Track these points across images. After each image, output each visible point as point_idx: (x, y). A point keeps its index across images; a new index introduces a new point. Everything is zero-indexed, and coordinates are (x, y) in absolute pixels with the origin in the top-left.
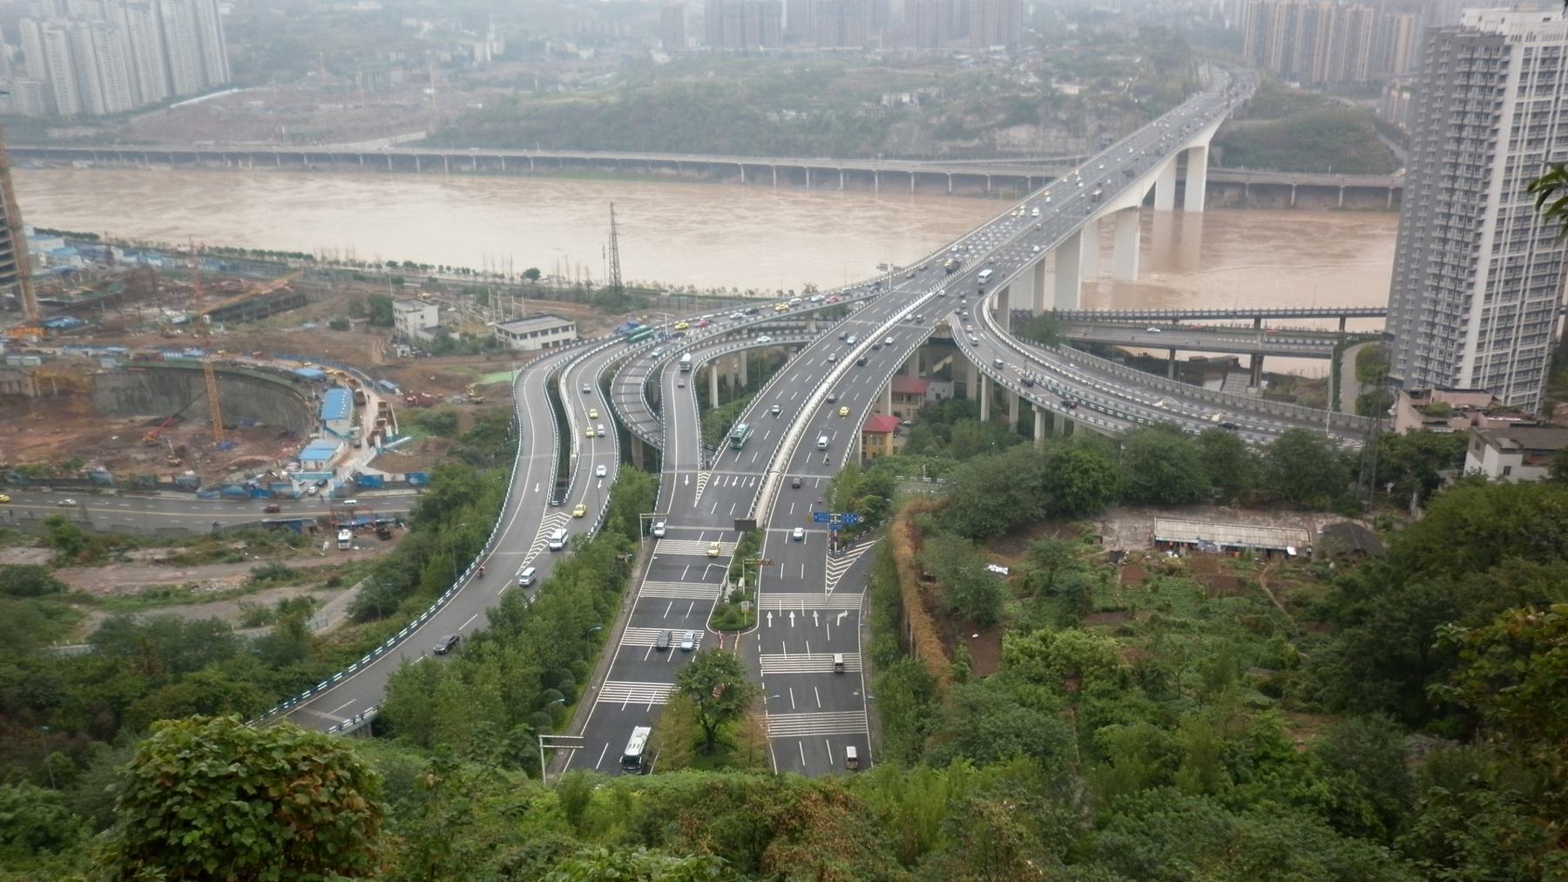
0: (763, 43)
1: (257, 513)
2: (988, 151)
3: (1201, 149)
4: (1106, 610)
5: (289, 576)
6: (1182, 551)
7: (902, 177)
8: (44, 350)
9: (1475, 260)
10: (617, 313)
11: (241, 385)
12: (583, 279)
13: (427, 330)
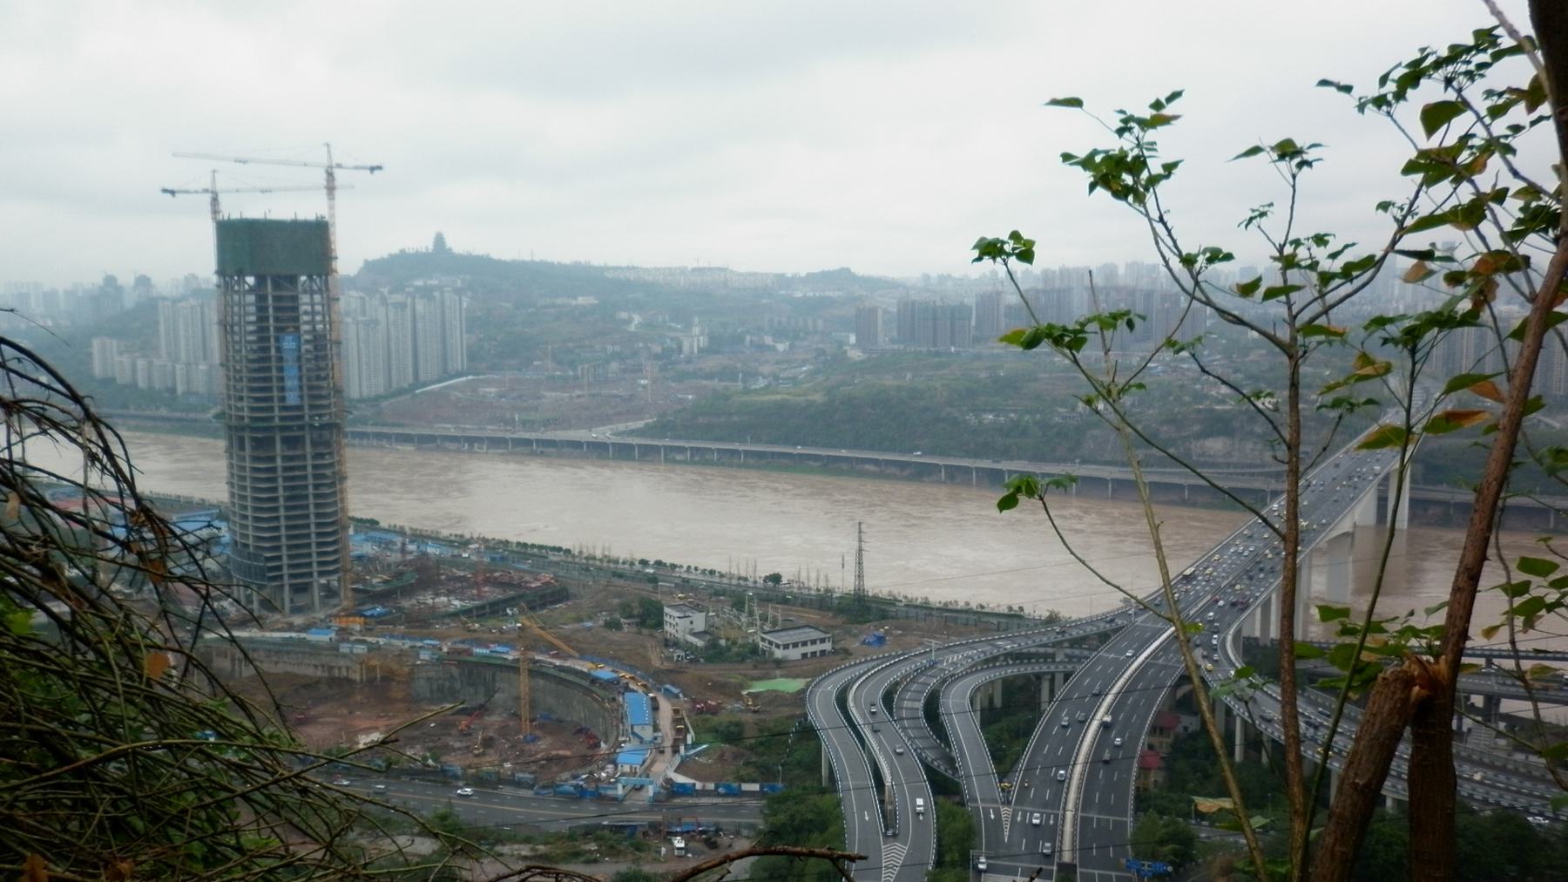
0: (953, 343)
1: (586, 813)
11: (541, 682)
12: (822, 585)
13: (695, 635)
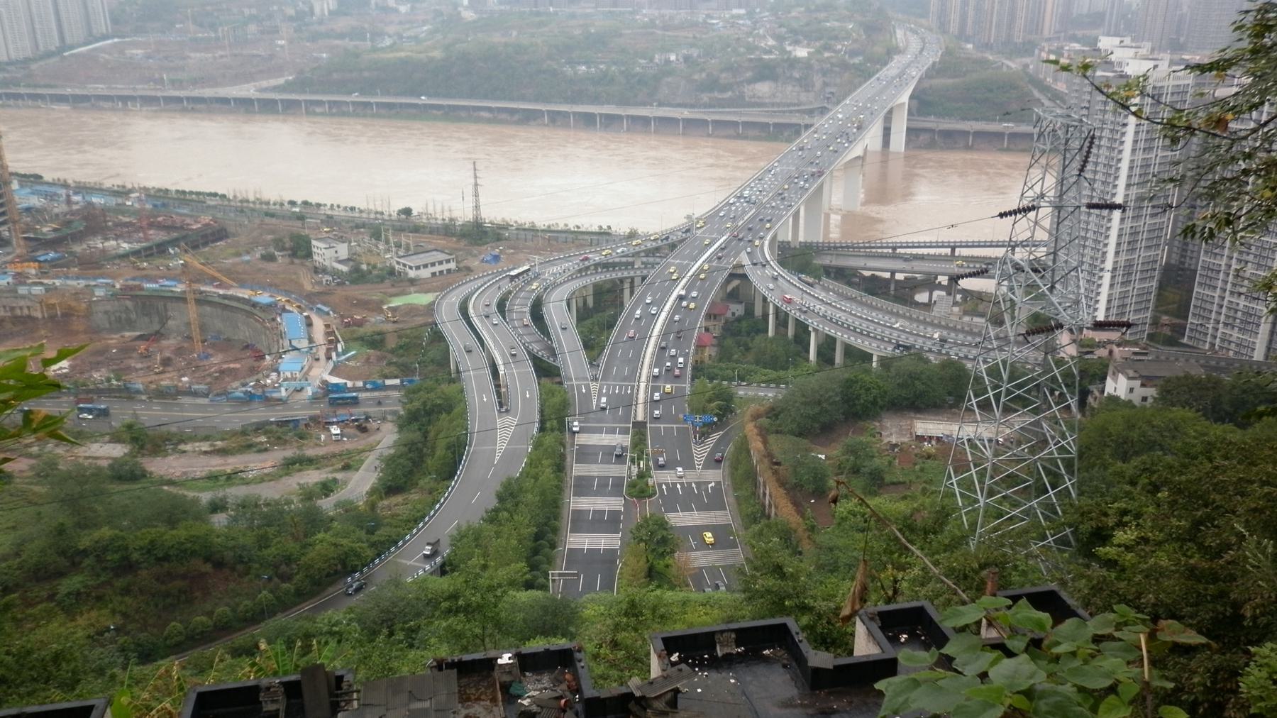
2: (740, 102)
4: (893, 484)
5: (310, 462)
6: (934, 442)
8: (46, 281)
9: (1108, 228)
10: (480, 245)
11: (208, 309)
12: (447, 215)
13: (340, 262)
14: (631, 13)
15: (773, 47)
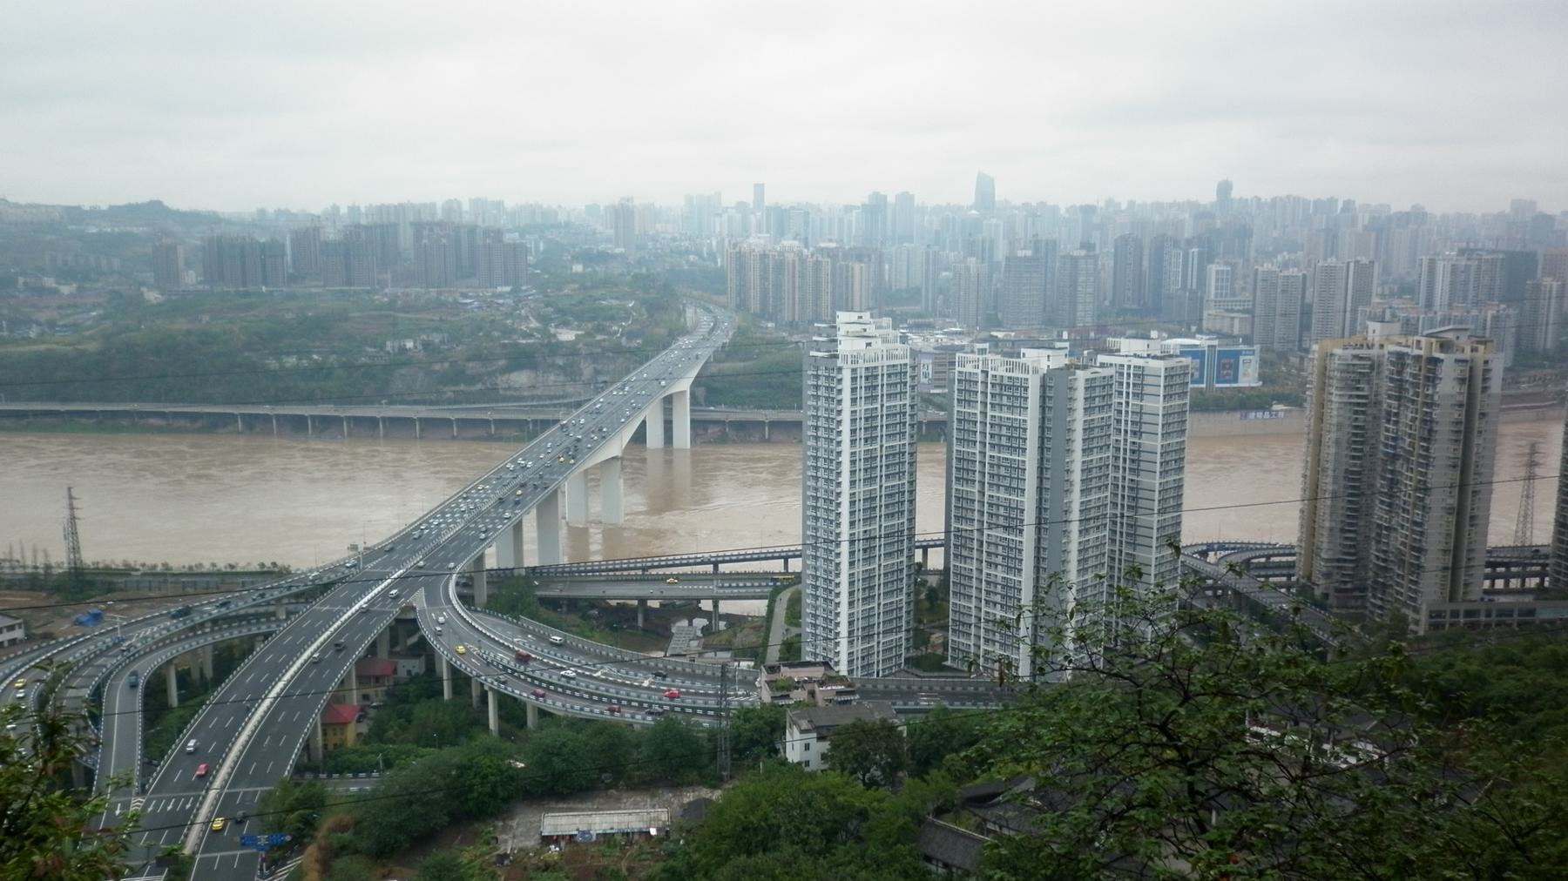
0: (265, 284)
2: (492, 395)
3: (684, 392)
7: (406, 422)
12: (41, 562)
14: (368, 292)
15: (537, 330)
